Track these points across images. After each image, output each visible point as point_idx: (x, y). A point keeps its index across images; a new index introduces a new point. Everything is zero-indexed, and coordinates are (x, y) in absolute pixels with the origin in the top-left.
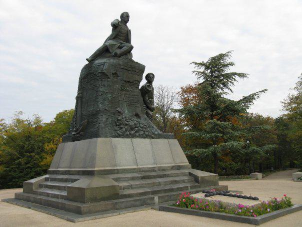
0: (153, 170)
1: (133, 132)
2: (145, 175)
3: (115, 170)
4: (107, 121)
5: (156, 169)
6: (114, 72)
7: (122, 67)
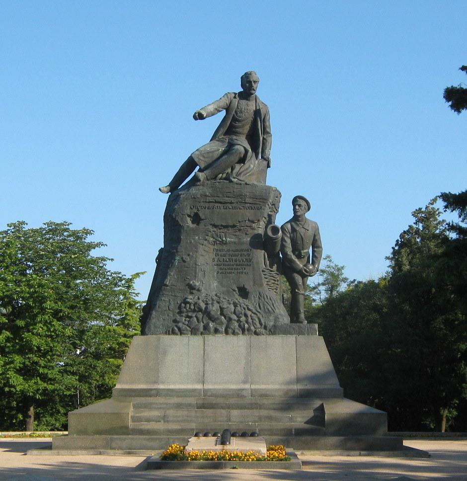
2: (208, 402)
3: (151, 390)
5: (244, 393)
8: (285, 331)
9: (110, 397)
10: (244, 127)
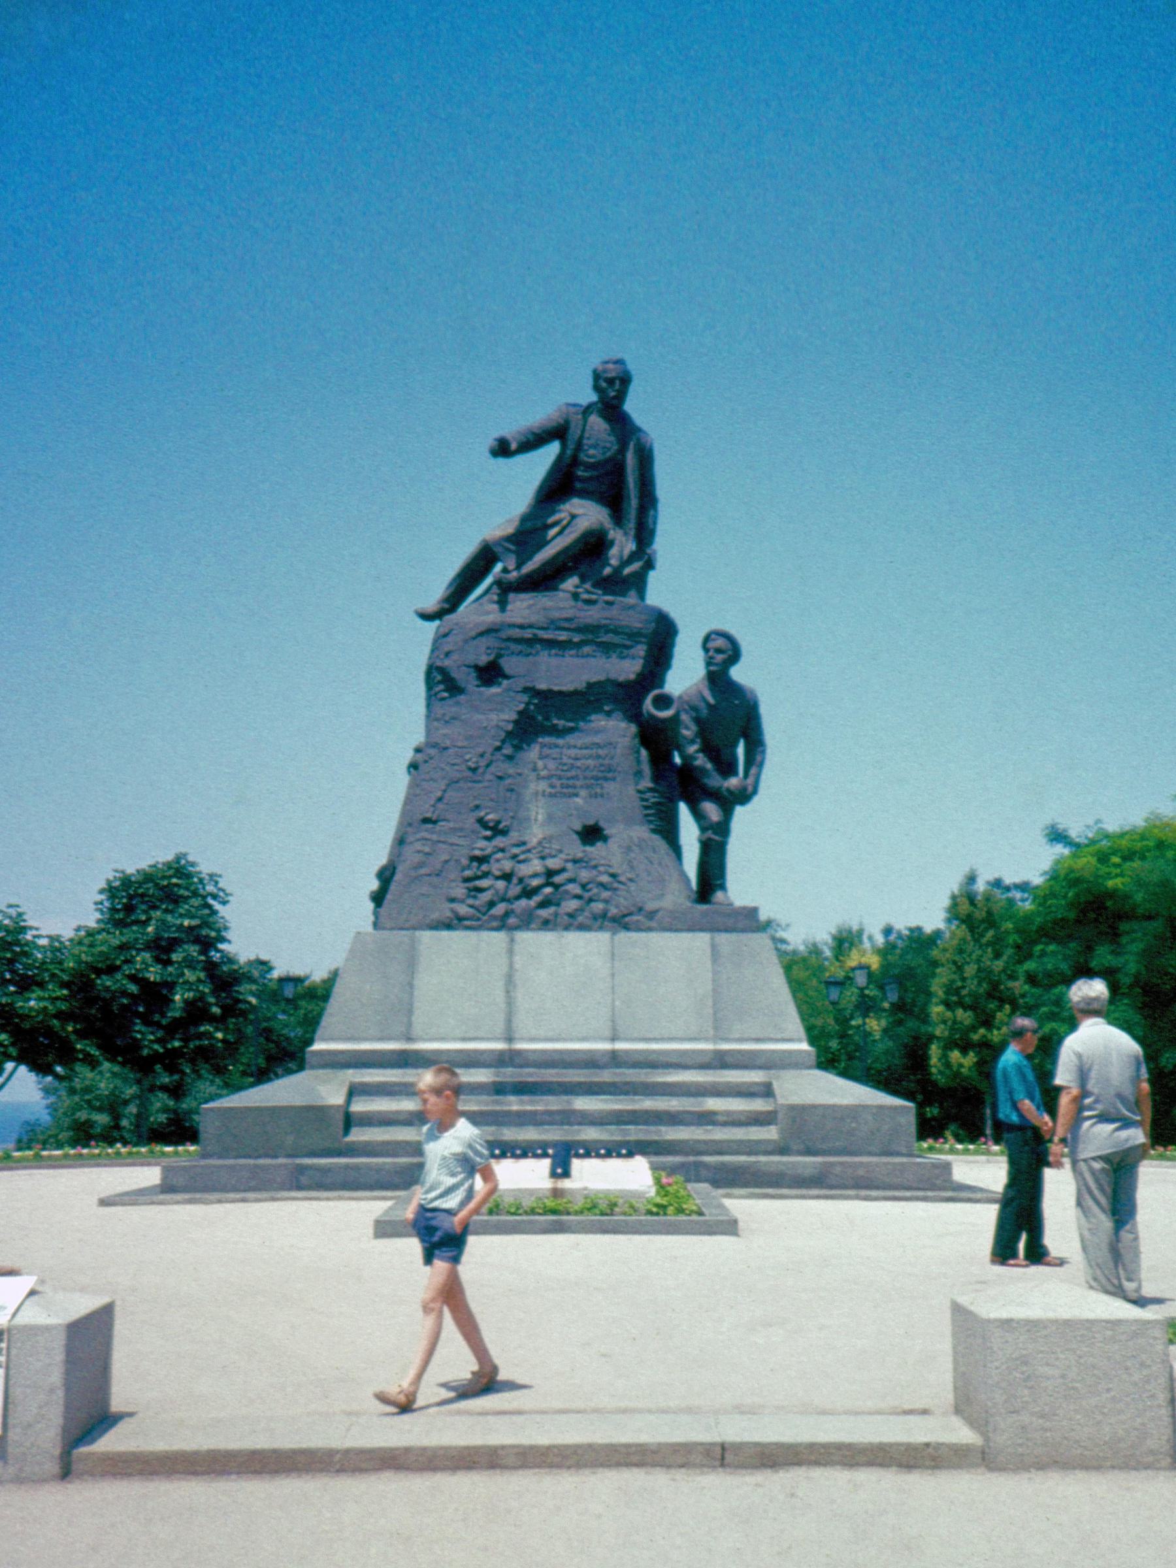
0: (590, 1061)
1: (523, 902)
4: (421, 865)
6: (484, 660)
7: (528, 634)
8: (676, 924)
9: (301, 1068)
10: (601, 470)
